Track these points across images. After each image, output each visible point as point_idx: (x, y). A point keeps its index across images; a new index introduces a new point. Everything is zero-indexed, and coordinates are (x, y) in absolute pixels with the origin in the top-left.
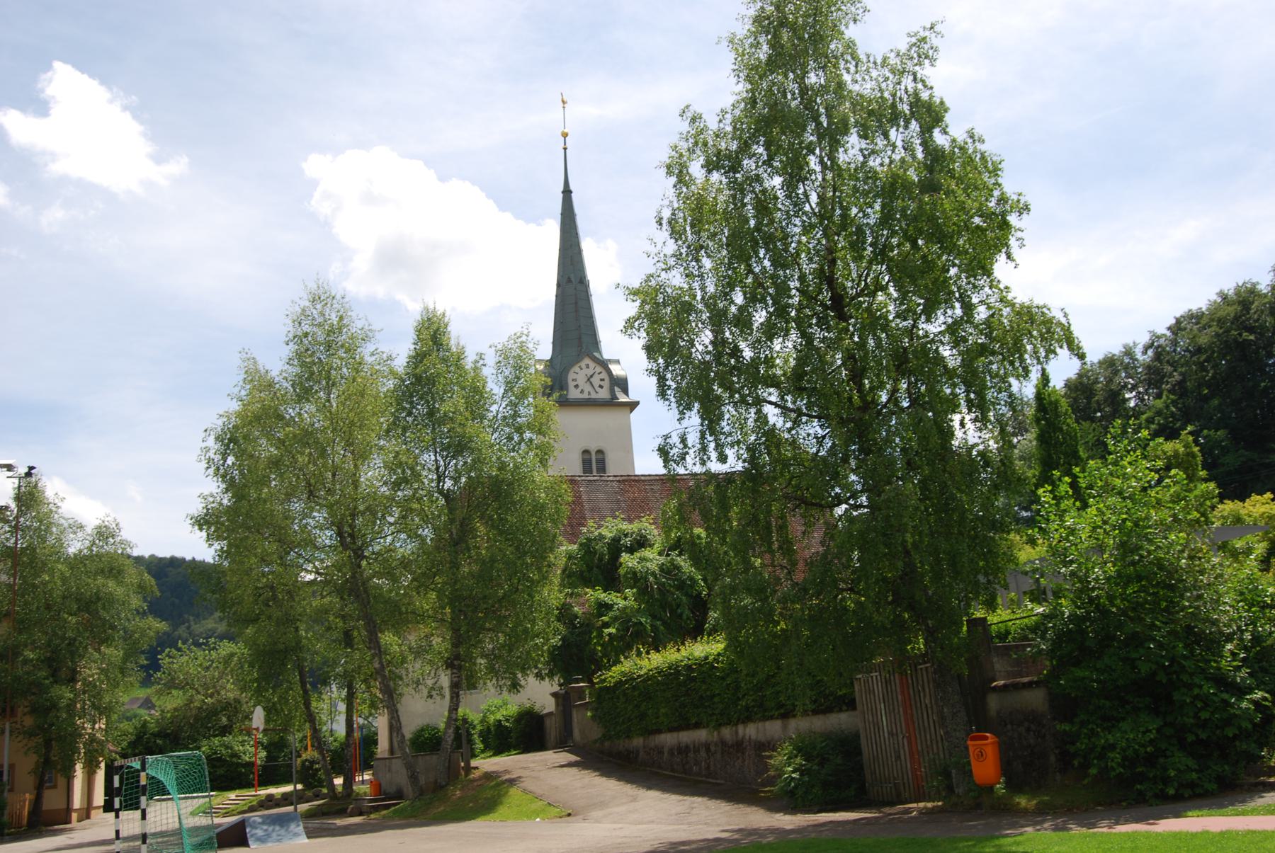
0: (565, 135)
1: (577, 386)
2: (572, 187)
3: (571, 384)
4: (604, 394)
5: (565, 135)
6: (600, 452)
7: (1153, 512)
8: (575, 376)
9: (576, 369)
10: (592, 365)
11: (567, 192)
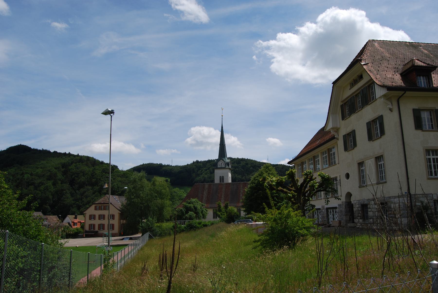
4: (224, 166)
6: (223, 177)
7: (210, 213)
11: (222, 127)
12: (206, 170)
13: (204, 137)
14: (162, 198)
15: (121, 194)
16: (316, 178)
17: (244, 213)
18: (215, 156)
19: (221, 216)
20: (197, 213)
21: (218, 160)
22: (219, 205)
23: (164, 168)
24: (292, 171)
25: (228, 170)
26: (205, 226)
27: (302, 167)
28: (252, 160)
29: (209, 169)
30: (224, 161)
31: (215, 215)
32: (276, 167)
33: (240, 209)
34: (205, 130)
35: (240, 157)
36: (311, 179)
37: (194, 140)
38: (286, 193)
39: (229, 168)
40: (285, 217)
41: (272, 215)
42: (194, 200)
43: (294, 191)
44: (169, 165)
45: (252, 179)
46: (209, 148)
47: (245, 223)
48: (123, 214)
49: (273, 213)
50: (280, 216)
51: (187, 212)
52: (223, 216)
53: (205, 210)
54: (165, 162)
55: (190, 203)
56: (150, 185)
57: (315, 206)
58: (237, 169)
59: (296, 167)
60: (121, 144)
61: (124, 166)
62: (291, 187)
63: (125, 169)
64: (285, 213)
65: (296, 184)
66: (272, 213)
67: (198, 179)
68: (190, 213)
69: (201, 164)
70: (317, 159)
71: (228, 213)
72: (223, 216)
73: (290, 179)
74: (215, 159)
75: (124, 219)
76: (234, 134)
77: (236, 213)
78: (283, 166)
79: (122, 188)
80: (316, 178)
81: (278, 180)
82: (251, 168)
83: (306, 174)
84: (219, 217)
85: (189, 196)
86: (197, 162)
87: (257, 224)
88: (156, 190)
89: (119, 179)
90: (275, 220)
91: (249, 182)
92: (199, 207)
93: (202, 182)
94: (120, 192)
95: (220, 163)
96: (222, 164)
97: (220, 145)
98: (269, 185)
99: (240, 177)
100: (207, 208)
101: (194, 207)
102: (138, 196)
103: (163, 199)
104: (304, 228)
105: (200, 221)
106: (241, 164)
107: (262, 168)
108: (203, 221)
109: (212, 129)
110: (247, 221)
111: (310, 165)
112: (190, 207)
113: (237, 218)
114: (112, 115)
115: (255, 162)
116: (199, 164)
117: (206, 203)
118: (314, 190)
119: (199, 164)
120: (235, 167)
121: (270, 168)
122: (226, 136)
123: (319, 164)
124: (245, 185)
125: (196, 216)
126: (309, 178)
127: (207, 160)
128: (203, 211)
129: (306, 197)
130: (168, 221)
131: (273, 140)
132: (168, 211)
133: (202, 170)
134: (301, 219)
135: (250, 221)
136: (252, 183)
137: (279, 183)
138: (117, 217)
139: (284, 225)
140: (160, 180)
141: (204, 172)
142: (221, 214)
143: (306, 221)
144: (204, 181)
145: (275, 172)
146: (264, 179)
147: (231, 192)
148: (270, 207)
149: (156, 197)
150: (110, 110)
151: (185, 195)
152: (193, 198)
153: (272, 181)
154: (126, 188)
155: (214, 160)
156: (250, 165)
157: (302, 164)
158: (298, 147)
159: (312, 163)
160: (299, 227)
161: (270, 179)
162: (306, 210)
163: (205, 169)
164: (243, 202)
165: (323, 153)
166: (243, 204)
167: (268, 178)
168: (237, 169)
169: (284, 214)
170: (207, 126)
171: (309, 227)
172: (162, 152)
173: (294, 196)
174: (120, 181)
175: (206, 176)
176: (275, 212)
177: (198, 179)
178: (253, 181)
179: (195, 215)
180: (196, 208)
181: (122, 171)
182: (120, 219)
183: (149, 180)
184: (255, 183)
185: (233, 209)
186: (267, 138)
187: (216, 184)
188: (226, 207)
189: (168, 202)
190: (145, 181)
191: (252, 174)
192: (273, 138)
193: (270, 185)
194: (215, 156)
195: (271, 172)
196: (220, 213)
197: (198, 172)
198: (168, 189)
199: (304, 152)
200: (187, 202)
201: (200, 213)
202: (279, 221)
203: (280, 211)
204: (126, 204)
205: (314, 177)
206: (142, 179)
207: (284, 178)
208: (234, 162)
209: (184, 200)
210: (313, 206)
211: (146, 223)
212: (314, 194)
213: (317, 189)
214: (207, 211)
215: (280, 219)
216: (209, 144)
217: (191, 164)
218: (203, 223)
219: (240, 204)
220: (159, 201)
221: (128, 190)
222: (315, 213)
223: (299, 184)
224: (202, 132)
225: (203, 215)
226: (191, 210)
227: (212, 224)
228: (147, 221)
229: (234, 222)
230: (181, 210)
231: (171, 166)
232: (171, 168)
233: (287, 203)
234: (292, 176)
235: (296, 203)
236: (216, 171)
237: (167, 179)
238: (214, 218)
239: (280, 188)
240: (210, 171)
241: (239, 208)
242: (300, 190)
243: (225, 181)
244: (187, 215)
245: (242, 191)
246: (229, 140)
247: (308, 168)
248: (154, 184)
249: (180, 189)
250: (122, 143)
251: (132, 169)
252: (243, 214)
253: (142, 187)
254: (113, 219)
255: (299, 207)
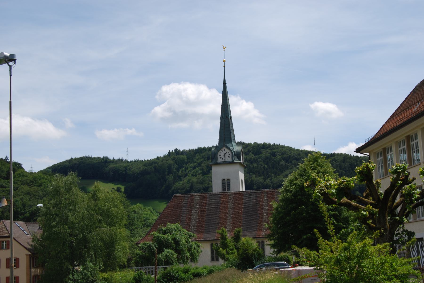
0: (224, 61)
1: (221, 157)
2: (226, 82)
3: (219, 157)
4: (230, 159)
5: (224, 61)
6: (228, 180)
7: (205, 250)
8: (220, 154)
9: (221, 151)
10: (226, 149)
11: (225, 84)
12: (194, 168)
13: (188, 103)
14: (111, 225)
15: (31, 217)
16: (414, 179)
17: (272, 250)
18: (212, 140)
19: (227, 256)
20: (179, 251)
21: (218, 148)
22: (222, 234)
23: (112, 166)
24: (367, 167)
25: (238, 167)
26: (197, 275)
27: (385, 158)
28: (283, 147)
29: (199, 165)
30: (229, 149)
31: (215, 255)
32: (332, 158)
33: (263, 242)
34: (190, 90)
35: (260, 141)
36: (406, 181)
37: (169, 110)
38: (356, 209)
39: (240, 163)
40: (357, 256)
41: (332, 252)
42: (173, 226)
43: (371, 204)
44: (122, 160)
45: (286, 183)
46: (198, 125)
47: (276, 270)
48: (36, 256)
49: (334, 249)
50: (347, 253)
51: (160, 251)
52: (231, 257)
53: (194, 246)
54: (114, 154)
55: (165, 233)
56: (86, 200)
57: (414, 234)
58: (255, 165)
59: (372, 158)
60: (28, 120)
61: (35, 162)
62: (366, 197)
63: (36, 169)
64: (356, 247)
65: (376, 191)
66: (331, 249)
67: (178, 185)
68: (167, 251)
69: (185, 157)
70: (414, 142)
71: (240, 251)
72: (231, 257)
73: (364, 183)
74: (211, 146)
75: (37, 267)
76: (247, 96)
77: (255, 250)
78: (345, 157)
79: (31, 206)
80: (414, 179)
81: (339, 185)
82: (283, 162)
83: (395, 172)
84: (223, 258)
85: (163, 219)
86: (177, 152)
87: (299, 271)
88: (99, 209)
89: (26, 188)
90: (338, 262)
91: (281, 190)
92: (183, 240)
93: (188, 192)
94: (28, 215)
95: (221, 153)
96: (227, 155)
97: (222, 118)
98: (322, 194)
99: (260, 179)
100: (199, 241)
101: (174, 239)
102: (65, 221)
103: (114, 225)
104: (396, 276)
105: (187, 266)
106: (263, 155)
107: (305, 164)
108: (191, 265)
109: (203, 88)
110: (278, 265)
111: (400, 153)
112: (167, 241)
113: (258, 259)
114: (11, 64)
115: (290, 149)
116: (181, 156)
117: (198, 232)
118: (411, 202)
119: (181, 156)
120: (251, 161)
121: (320, 160)
122: (231, 100)
123: (418, 152)
124: (272, 196)
125: (178, 257)
126: (401, 178)
127: (195, 147)
128: (191, 246)
129: (395, 215)
130: (123, 267)
131: (324, 107)
132: (123, 250)
133: (186, 169)
134: (389, 259)
135: (284, 265)
136: (286, 191)
137: (343, 191)
138: (24, 263)
139: (355, 271)
140: (105, 189)
141: (190, 172)
142: (228, 253)
143: (399, 262)
144: (191, 189)
145: (331, 169)
146: (314, 183)
147: (245, 209)
148: (327, 237)
149: (100, 221)
150: (8, 55)
151: (156, 218)
152: (171, 223)
153: (329, 187)
154: (41, 205)
155: (210, 149)
156: (279, 157)
157: (385, 151)
158: (376, 118)
159: (404, 149)
160: (385, 274)
161: (324, 182)
162: (397, 242)
163: (192, 165)
164: (270, 228)
165: (399, 144)
166: (269, 232)
167: (319, 182)
168: (255, 165)
169: (354, 251)
170: (192, 81)
171: (404, 275)
172: (107, 134)
173: (372, 215)
174: (28, 193)
175: (194, 179)
176: (338, 245)
177: (178, 185)
178: (287, 187)
179: (175, 255)
180: (177, 242)
181: (31, 173)
182: (30, 267)
183: (84, 189)
184: (291, 192)
185: (249, 241)
186: (312, 102)
187: (216, 194)
188: (237, 238)
189: (123, 232)
190: (76, 190)
191: (284, 173)
192: (324, 102)
193: (325, 195)
194: (212, 140)
195: (322, 170)
196: (224, 251)
197: (178, 171)
198: (121, 207)
199: (389, 128)
200: (161, 231)
201: (186, 251)
202: (345, 264)
203: (346, 244)
204: (42, 236)
205: (410, 178)
206: (70, 189)
207: (353, 181)
208: (249, 151)
209: (154, 227)
210: (411, 234)
211: (82, 272)
212: (413, 211)
213: (417, 200)
214: (199, 246)
215: (348, 259)
216: (197, 116)
217: (164, 156)
218: (192, 271)
219: (264, 233)
220: (106, 230)
221: (44, 209)
222: (413, 248)
223: (382, 191)
224: (183, 94)
225: (192, 255)
226: (168, 246)
227: (210, 272)
228: (84, 269)
229: (252, 268)
230: (149, 246)
231: (126, 161)
232: (125, 165)
233: (359, 229)
234: (367, 175)
235: (375, 229)
236: (215, 169)
237: (119, 186)
238: (213, 259)
239: (345, 200)
240: (202, 169)
241: (260, 240)
242: (384, 203)
243: (233, 189)
244: (160, 256)
245: (266, 207)
246: (239, 108)
247: (398, 160)
248: (95, 197)
249: (145, 205)
250: (30, 120)
251: (49, 168)
252: (269, 251)
253: (72, 203)
254: (17, 266)
255: (382, 235)
